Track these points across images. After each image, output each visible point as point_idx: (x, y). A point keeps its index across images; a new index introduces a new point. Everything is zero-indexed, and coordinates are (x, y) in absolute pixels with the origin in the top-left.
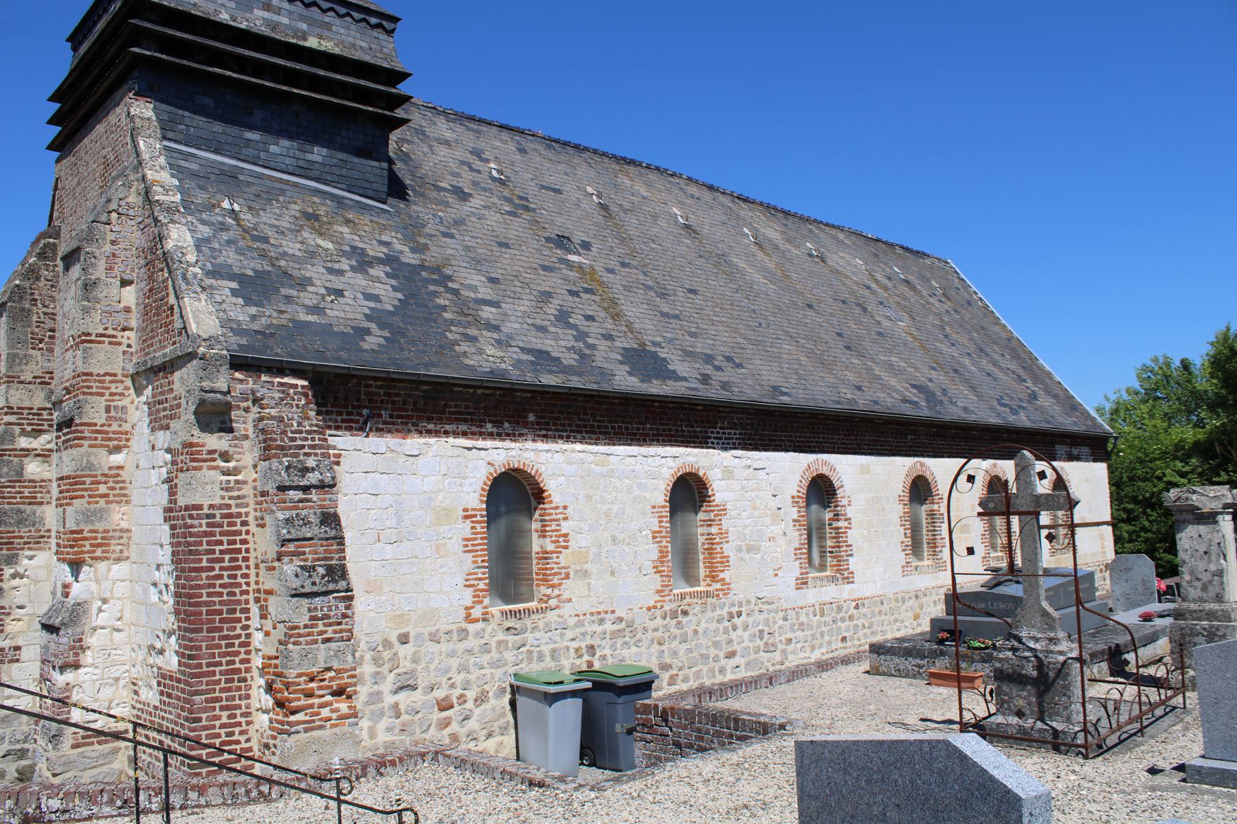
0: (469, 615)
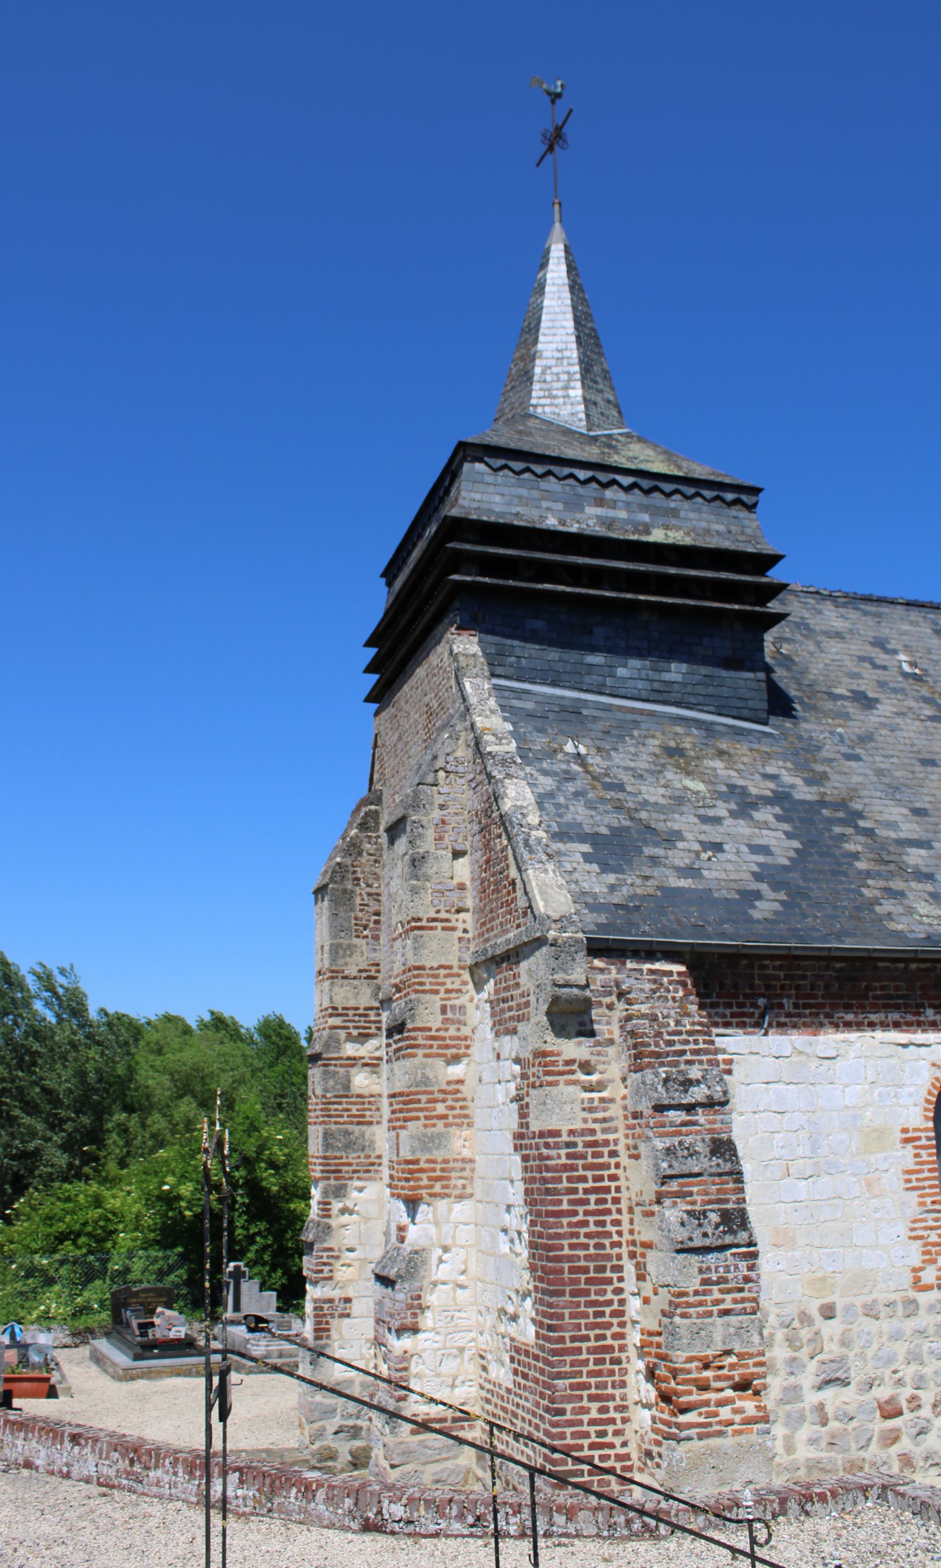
0: (917, 1280)
